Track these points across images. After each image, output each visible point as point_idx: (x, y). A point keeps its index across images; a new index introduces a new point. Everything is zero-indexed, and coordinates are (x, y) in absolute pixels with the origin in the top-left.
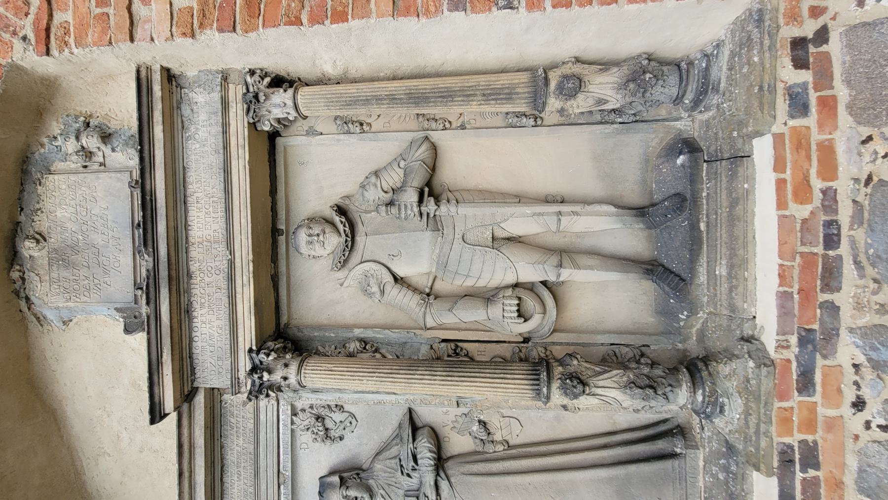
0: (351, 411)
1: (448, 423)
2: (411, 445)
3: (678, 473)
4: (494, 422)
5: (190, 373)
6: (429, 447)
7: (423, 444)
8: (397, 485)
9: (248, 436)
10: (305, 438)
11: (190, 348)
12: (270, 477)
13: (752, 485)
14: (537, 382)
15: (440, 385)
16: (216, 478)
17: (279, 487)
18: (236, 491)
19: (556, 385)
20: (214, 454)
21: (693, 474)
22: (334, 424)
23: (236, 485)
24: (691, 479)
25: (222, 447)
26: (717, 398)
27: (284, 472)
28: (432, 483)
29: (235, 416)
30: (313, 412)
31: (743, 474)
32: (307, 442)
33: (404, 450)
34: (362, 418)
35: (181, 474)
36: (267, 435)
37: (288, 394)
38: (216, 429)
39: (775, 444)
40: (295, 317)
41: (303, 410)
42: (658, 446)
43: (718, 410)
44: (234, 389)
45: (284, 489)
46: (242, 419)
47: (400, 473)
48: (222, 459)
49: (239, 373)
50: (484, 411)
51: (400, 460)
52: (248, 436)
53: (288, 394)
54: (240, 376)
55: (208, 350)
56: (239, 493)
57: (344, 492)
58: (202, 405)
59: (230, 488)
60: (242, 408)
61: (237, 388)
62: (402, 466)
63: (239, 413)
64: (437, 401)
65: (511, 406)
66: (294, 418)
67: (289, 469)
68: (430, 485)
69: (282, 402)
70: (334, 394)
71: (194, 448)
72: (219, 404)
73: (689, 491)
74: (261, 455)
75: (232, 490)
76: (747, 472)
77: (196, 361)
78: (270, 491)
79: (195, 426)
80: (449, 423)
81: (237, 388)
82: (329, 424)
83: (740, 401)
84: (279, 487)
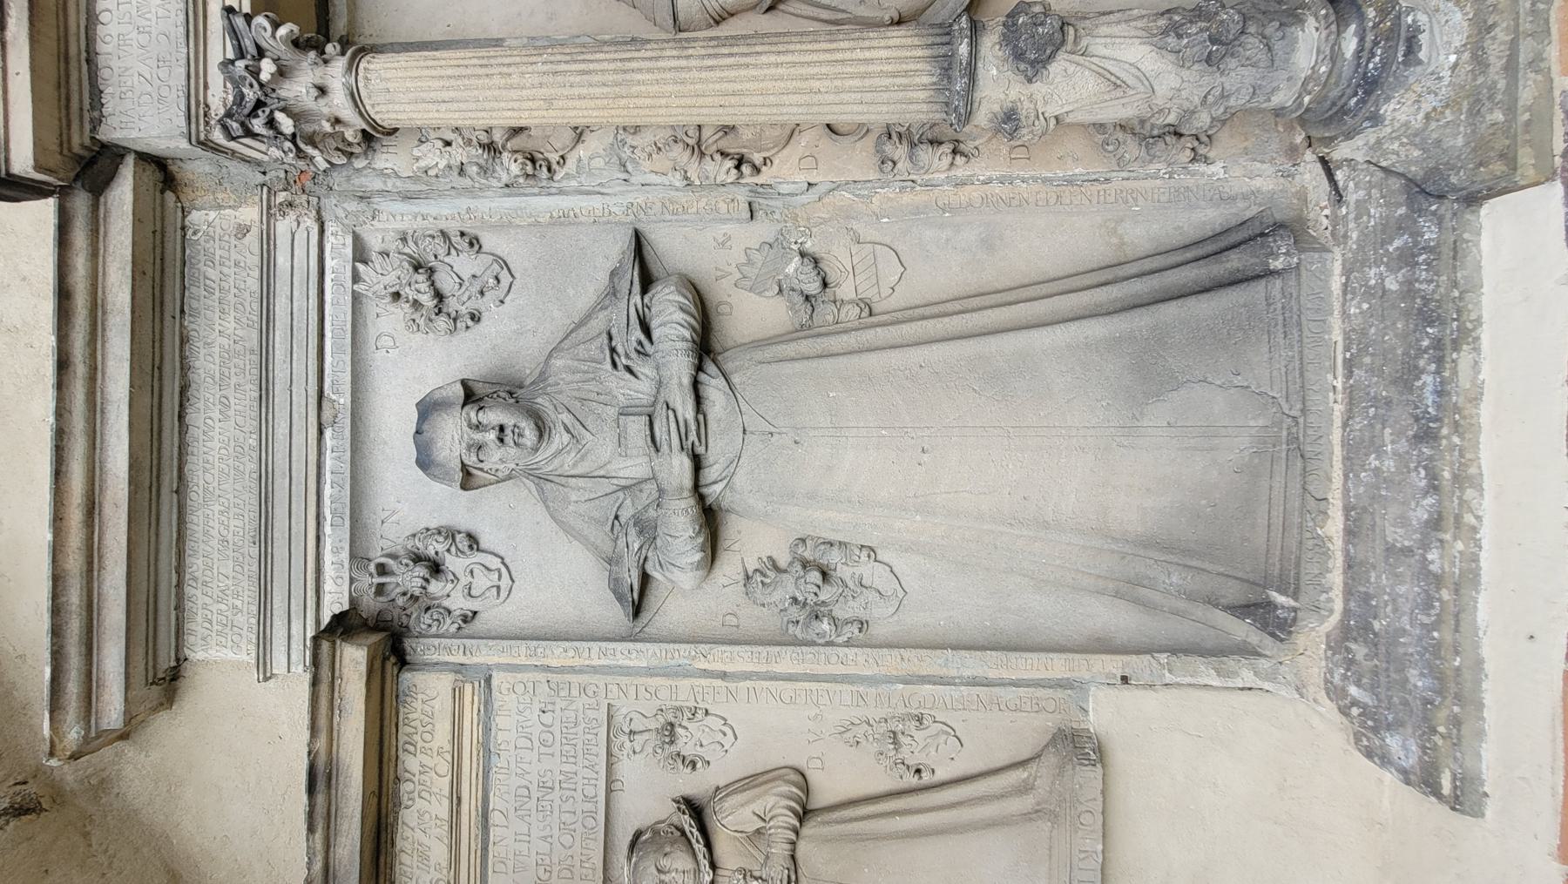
0: (499, 252)
1: (729, 269)
2: (637, 299)
3: (1279, 311)
4: (838, 257)
5: (87, 101)
6: (679, 302)
7: (667, 297)
8: (602, 398)
9: (249, 309)
10: (387, 321)
11: (90, 40)
12: (300, 406)
13: (1478, 268)
14: (946, 39)
15: (701, 69)
16: (167, 406)
17: (321, 432)
18: (216, 444)
19: (990, 44)
20: (161, 347)
21: (1318, 311)
22: (457, 280)
23: (217, 430)
24: (1312, 325)
25: (184, 340)
26: (1398, 17)
27: (334, 397)
28: (686, 381)
29: (217, 263)
30: (407, 250)
31: (1455, 242)
32: (393, 332)
33: (619, 316)
34: (526, 270)
35: (63, 364)
36: (292, 304)
37: (345, 205)
38: (168, 289)
39: (1557, 93)
40: (367, 33)
41: (385, 254)
42: (1228, 265)
43: (1402, 49)
44: (193, 126)
45: (333, 438)
46: (233, 269)
47: (608, 366)
48: (185, 368)
49: (210, 93)
50: (814, 230)
51: (610, 338)
52: (249, 309)
53: (345, 205)
54: (210, 100)
55: (135, 44)
56: (223, 451)
57: (473, 414)
58: (128, 207)
59: (202, 437)
60: (233, 241)
61: (202, 128)
62: (613, 350)
63: (226, 254)
64: (702, 204)
65: (878, 211)
66: (360, 267)
67: (347, 388)
68: (680, 384)
69: (330, 228)
70: (457, 202)
71: (104, 313)
72: (179, 232)
73: (1309, 354)
74: (277, 352)
75: (208, 444)
76: (1466, 236)
77: (104, 73)
78: (298, 439)
79: (109, 259)
80: (733, 269)
81: (202, 128)
82: (446, 282)
83: (1459, 16)
84: (321, 432)
